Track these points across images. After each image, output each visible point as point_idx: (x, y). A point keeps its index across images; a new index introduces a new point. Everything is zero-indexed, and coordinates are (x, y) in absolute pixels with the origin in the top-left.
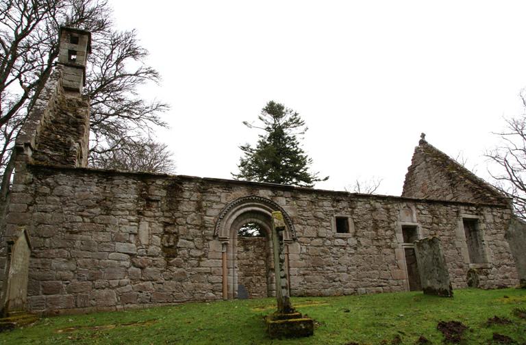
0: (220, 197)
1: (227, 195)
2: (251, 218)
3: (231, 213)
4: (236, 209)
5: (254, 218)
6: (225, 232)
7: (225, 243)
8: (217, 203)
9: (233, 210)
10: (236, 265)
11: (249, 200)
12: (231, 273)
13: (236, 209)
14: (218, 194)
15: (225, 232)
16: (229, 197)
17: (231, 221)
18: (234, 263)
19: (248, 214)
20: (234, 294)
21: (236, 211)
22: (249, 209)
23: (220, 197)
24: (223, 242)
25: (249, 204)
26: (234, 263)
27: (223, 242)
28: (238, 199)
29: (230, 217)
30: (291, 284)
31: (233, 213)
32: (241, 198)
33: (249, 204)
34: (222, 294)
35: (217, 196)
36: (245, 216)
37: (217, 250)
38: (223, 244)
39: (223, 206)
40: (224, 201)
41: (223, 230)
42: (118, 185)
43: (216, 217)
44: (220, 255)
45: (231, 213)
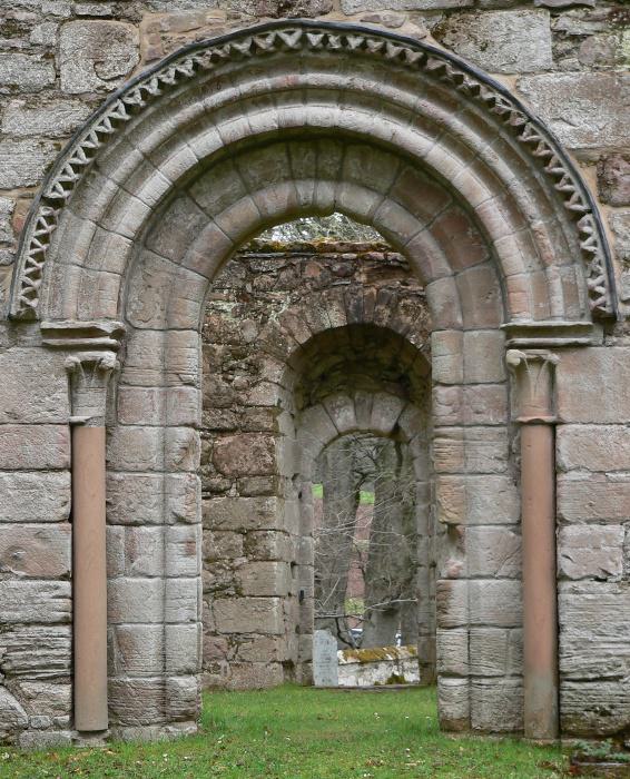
0: (50, 54)
1: (109, 38)
2: (292, 177)
3: (130, 159)
4: (168, 125)
5: (319, 176)
6: (89, 289)
7: (89, 366)
8: (33, 97)
9: (148, 141)
10: (179, 505)
11: (262, 61)
12: (149, 558)
13: (168, 125)
14: (37, 35)
15: (89, 289)
16: (115, 52)
17: (133, 213)
18: (165, 493)
19: (276, 155)
20: (165, 695)
21: (170, 142)
22: (263, 119)
23: (50, 54)
24: (74, 359)
25: (264, 83)
26: (165, 493)
27: (74, 359)
28: (179, 56)
29: (126, 187)
30: (569, 635)
31: (152, 159)
32: (198, 47)
33: (264, 83)
34: (65, 691)
35: (29, 50)
36: (253, 171)
37: (28, 413)
38: (72, 375)
39: (76, 114)
40: (79, 77)
41: (538, 224)
42: (138, 47)
43: (26, 191)
44: (53, 447)
45: (130, 159)
